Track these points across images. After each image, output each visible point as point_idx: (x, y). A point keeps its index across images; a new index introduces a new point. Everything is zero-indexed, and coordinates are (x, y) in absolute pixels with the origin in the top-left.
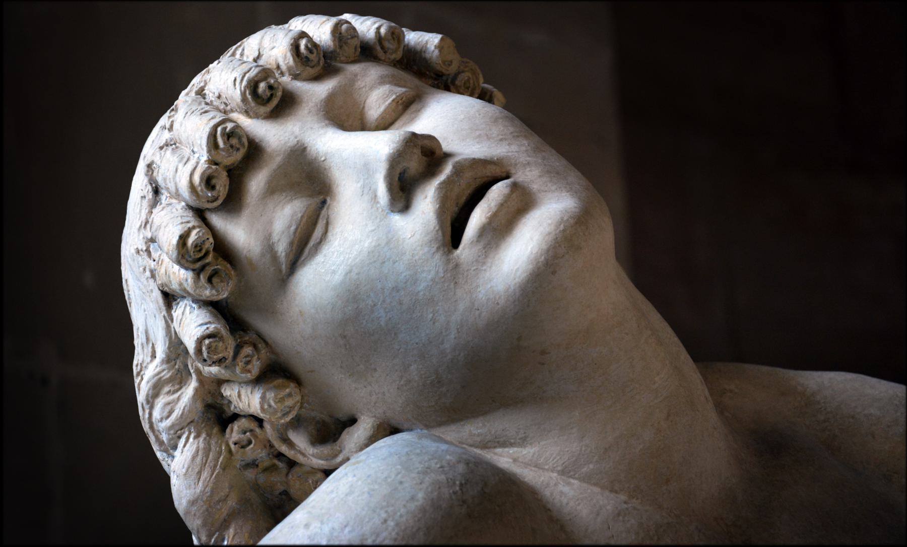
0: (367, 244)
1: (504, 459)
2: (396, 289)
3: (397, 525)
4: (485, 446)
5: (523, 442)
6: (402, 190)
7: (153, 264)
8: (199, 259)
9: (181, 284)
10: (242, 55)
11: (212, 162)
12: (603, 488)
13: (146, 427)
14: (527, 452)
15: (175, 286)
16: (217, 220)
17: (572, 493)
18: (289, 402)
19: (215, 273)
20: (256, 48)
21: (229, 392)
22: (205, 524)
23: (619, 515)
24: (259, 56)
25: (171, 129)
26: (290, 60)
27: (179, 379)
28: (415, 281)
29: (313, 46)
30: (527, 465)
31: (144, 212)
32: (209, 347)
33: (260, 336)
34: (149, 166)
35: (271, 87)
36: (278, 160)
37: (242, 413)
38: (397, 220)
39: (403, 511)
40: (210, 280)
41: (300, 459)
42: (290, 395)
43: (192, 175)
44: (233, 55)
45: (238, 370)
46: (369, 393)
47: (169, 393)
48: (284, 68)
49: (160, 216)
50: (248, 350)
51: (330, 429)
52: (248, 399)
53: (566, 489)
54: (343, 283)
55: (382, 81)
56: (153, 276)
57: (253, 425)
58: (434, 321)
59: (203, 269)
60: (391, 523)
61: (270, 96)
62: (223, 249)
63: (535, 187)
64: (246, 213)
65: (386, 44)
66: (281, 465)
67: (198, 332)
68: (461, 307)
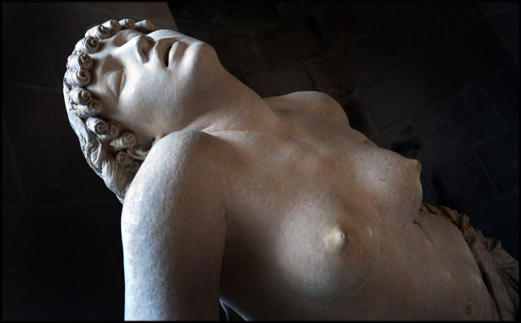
0: (139, 76)
1: (206, 131)
2: (153, 86)
3: (175, 154)
5: (209, 124)
6: (145, 54)
8: (87, 100)
9: (84, 111)
11: (82, 68)
12: (240, 130)
13: (91, 166)
14: (212, 127)
16: (90, 88)
17: (230, 135)
18: (132, 139)
19: (94, 104)
21: (112, 144)
22: (118, 189)
23: (247, 136)
26: (99, 33)
28: (158, 82)
30: (213, 131)
32: (99, 128)
33: (116, 121)
35: (95, 42)
36: (104, 61)
37: (119, 150)
38: (147, 65)
39: (176, 149)
40: (93, 106)
42: (131, 137)
43: (77, 74)
45: (112, 133)
47: (94, 151)
48: (98, 37)
49: (72, 92)
50: (113, 126)
52: (119, 143)
53: (228, 134)
54: (135, 91)
56: (77, 115)
57: (124, 153)
58: (168, 92)
59: (90, 103)
60: (173, 154)
62: (95, 96)
64: (98, 81)
65: (130, 25)
66: (136, 163)
67: (95, 124)
68: (175, 84)
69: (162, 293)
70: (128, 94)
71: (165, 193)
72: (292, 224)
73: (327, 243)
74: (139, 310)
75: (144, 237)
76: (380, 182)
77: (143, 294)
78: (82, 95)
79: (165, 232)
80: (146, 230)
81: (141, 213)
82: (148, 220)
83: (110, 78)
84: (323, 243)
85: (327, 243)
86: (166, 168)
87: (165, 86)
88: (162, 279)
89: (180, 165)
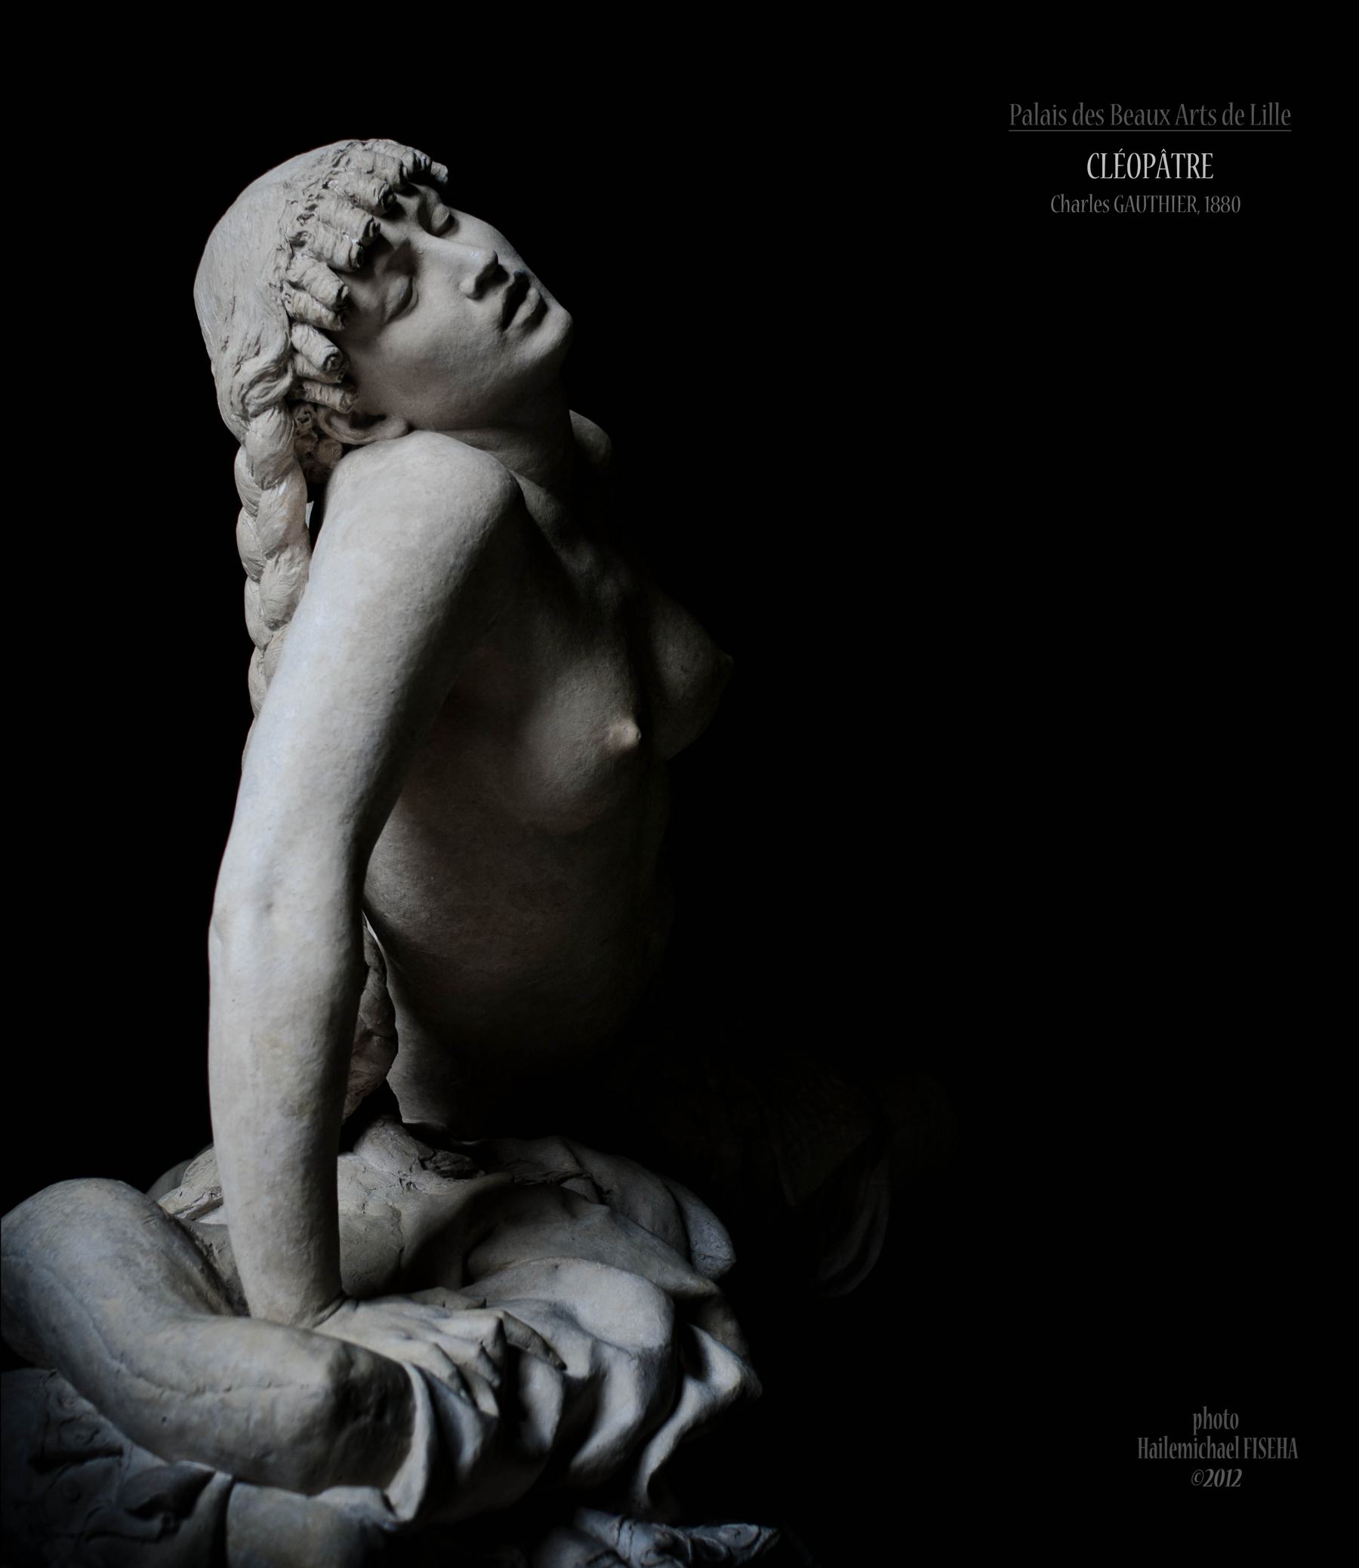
2: (465, 347)
6: (482, 289)
32: (333, 363)
51: (367, 420)
70: (406, 336)
71: (457, 556)
73: (611, 735)
75: (402, 608)
76: (679, 671)
77: (353, 692)
80: (408, 600)
82: (418, 585)
83: (396, 287)
84: (607, 733)
87: (485, 358)
88: (396, 684)
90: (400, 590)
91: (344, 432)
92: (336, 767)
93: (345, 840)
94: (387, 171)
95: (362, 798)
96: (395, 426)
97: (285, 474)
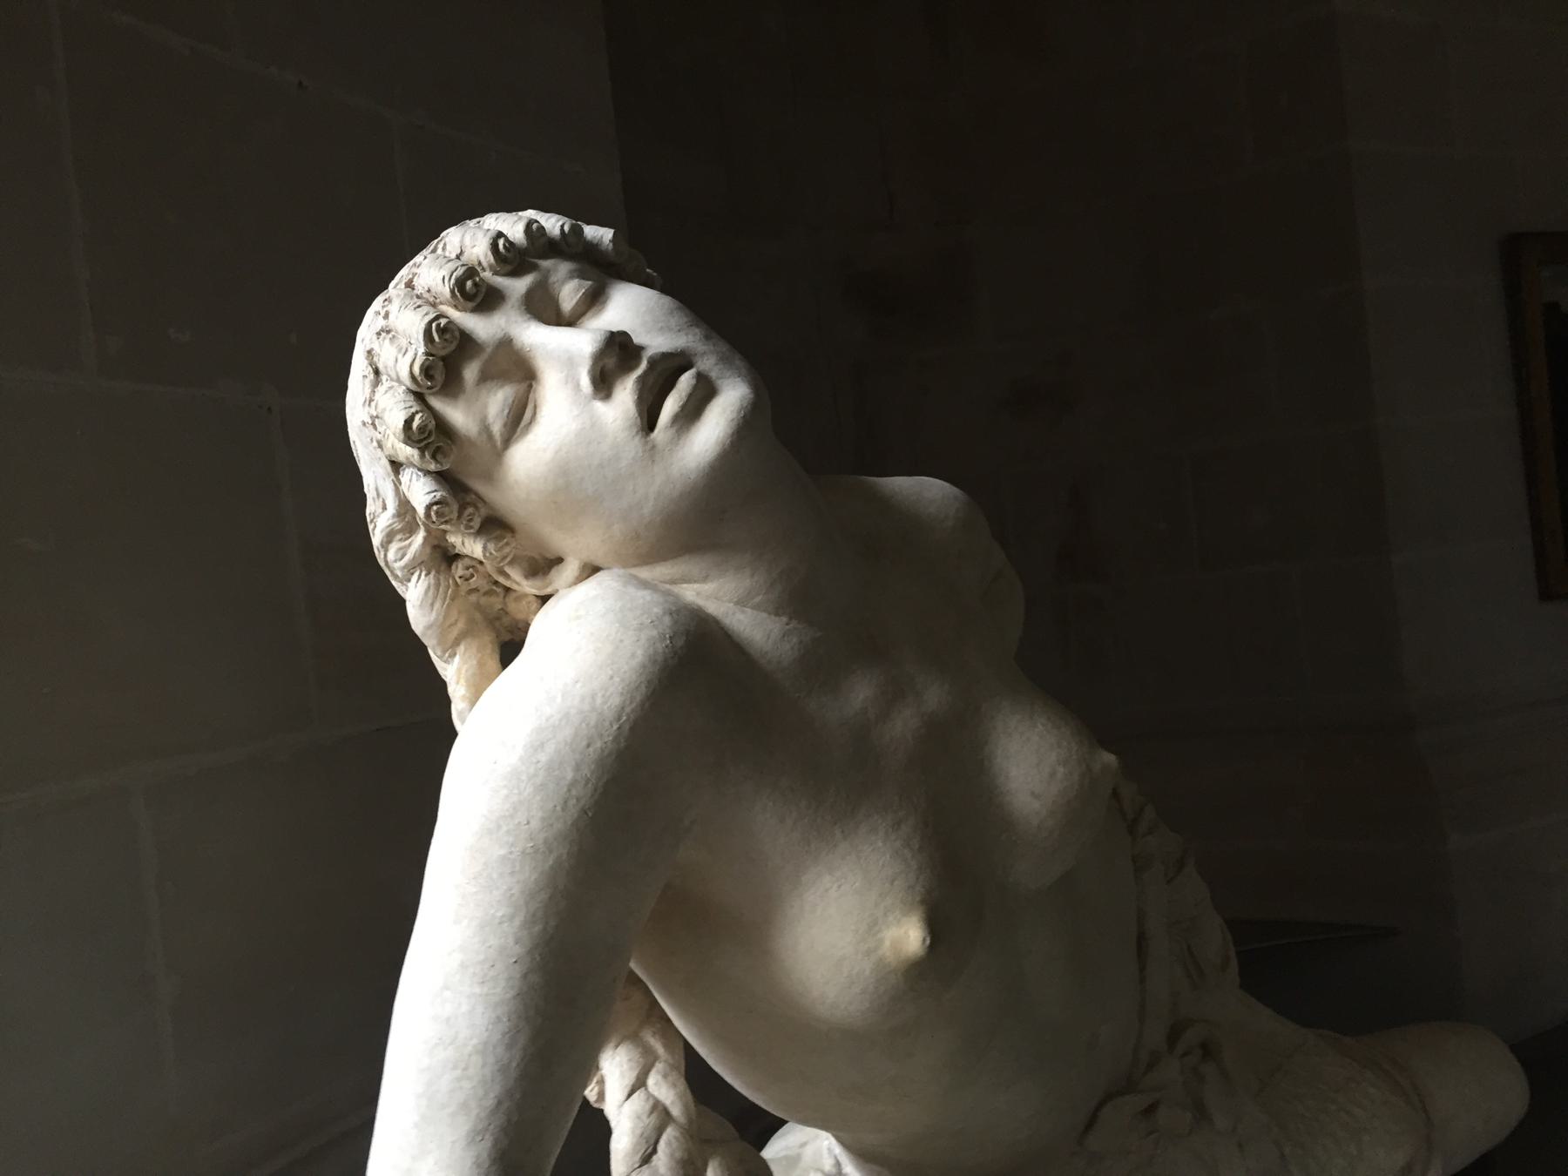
0: (574, 426)
2: (601, 466)
4: (673, 582)
6: (603, 383)
7: (379, 437)
10: (444, 249)
11: (427, 354)
13: (382, 564)
15: (401, 459)
16: (437, 403)
19: (438, 448)
20: (458, 245)
24: (462, 252)
25: (386, 316)
27: (410, 529)
29: (510, 245)
31: (368, 390)
32: (437, 513)
33: (477, 494)
34: (369, 352)
35: (475, 284)
36: (489, 350)
38: (599, 406)
40: (434, 457)
41: (515, 587)
44: (434, 251)
46: (576, 544)
48: (485, 264)
50: (470, 510)
51: (543, 565)
52: (474, 548)
55: (571, 276)
56: (380, 446)
59: (427, 446)
60: (617, 679)
61: (475, 292)
63: (713, 375)
67: (428, 499)
69: (510, 979)
70: (531, 460)
71: (577, 768)
72: (827, 879)
73: (887, 943)
74: (447, 994)
75: (502, 852)
77: (463, 966)
78: (415, 425)
79: (555, 854)
81: (507, 796)
82: (521, 817)
83: (497, 401)
84: (881, 941)
85: (887, 943)
86: (593, 709)
88: (518, 950)
89: (628, 710)
90: (499, 827)
91: (528, 587)
92: (455, 1068)
93: (479, 1166)
94: (475, 250)
95: (499, 1103)
96: (570, 569)
97: (457, 643)
